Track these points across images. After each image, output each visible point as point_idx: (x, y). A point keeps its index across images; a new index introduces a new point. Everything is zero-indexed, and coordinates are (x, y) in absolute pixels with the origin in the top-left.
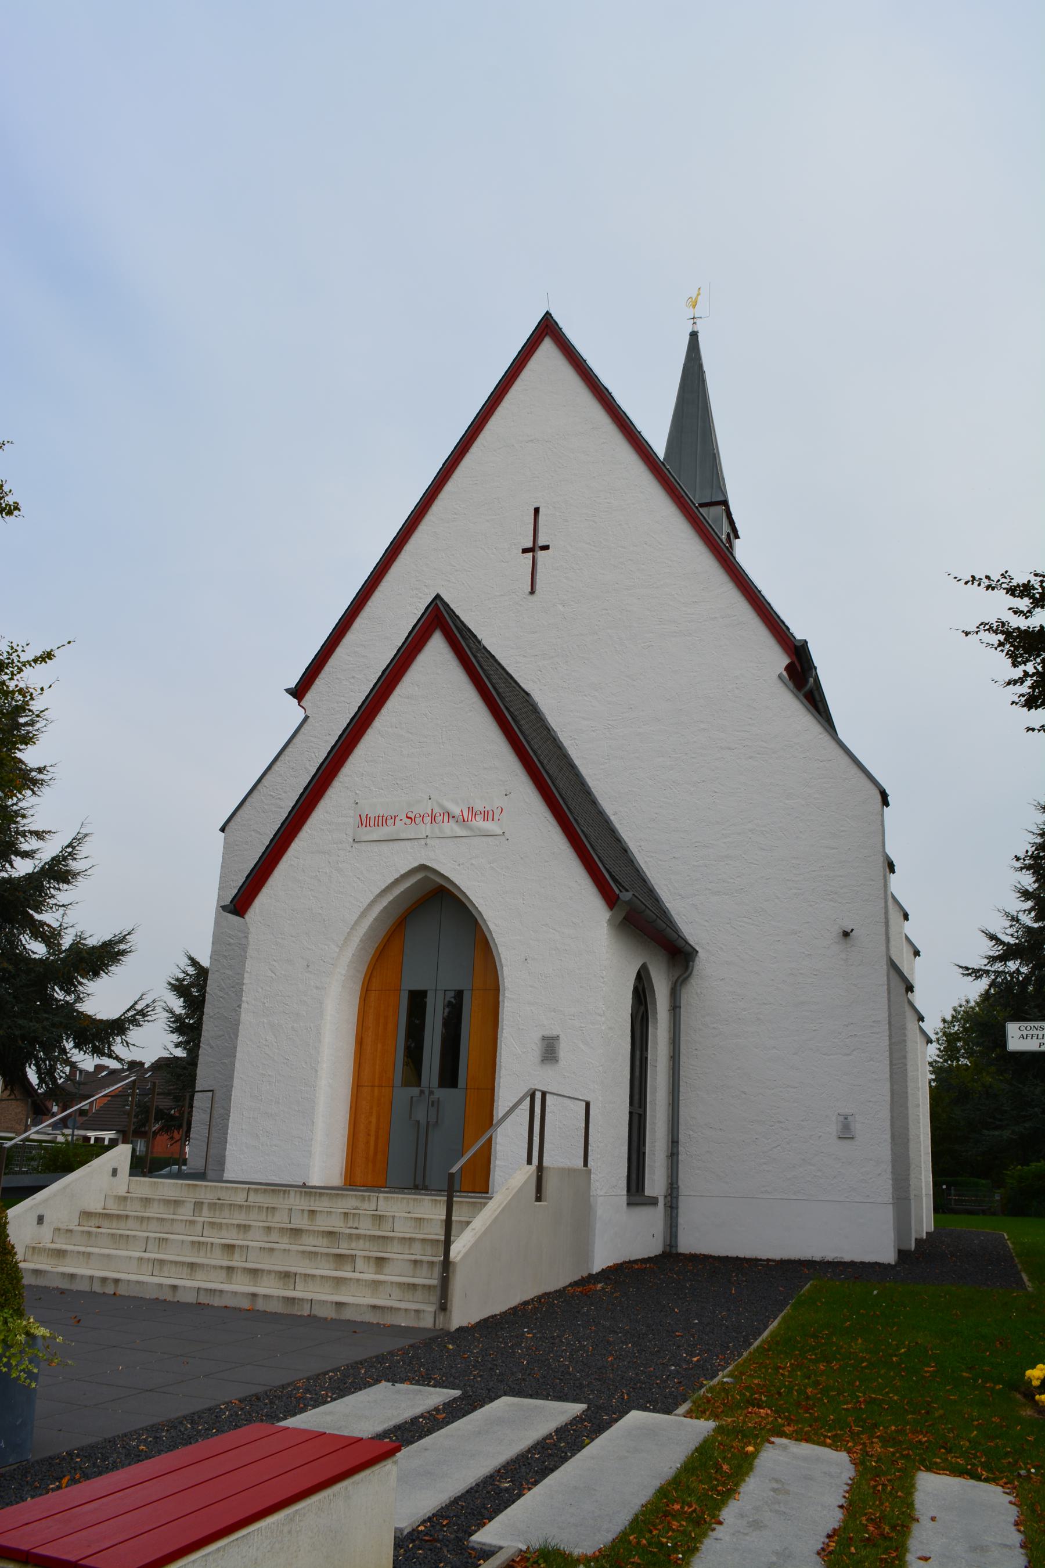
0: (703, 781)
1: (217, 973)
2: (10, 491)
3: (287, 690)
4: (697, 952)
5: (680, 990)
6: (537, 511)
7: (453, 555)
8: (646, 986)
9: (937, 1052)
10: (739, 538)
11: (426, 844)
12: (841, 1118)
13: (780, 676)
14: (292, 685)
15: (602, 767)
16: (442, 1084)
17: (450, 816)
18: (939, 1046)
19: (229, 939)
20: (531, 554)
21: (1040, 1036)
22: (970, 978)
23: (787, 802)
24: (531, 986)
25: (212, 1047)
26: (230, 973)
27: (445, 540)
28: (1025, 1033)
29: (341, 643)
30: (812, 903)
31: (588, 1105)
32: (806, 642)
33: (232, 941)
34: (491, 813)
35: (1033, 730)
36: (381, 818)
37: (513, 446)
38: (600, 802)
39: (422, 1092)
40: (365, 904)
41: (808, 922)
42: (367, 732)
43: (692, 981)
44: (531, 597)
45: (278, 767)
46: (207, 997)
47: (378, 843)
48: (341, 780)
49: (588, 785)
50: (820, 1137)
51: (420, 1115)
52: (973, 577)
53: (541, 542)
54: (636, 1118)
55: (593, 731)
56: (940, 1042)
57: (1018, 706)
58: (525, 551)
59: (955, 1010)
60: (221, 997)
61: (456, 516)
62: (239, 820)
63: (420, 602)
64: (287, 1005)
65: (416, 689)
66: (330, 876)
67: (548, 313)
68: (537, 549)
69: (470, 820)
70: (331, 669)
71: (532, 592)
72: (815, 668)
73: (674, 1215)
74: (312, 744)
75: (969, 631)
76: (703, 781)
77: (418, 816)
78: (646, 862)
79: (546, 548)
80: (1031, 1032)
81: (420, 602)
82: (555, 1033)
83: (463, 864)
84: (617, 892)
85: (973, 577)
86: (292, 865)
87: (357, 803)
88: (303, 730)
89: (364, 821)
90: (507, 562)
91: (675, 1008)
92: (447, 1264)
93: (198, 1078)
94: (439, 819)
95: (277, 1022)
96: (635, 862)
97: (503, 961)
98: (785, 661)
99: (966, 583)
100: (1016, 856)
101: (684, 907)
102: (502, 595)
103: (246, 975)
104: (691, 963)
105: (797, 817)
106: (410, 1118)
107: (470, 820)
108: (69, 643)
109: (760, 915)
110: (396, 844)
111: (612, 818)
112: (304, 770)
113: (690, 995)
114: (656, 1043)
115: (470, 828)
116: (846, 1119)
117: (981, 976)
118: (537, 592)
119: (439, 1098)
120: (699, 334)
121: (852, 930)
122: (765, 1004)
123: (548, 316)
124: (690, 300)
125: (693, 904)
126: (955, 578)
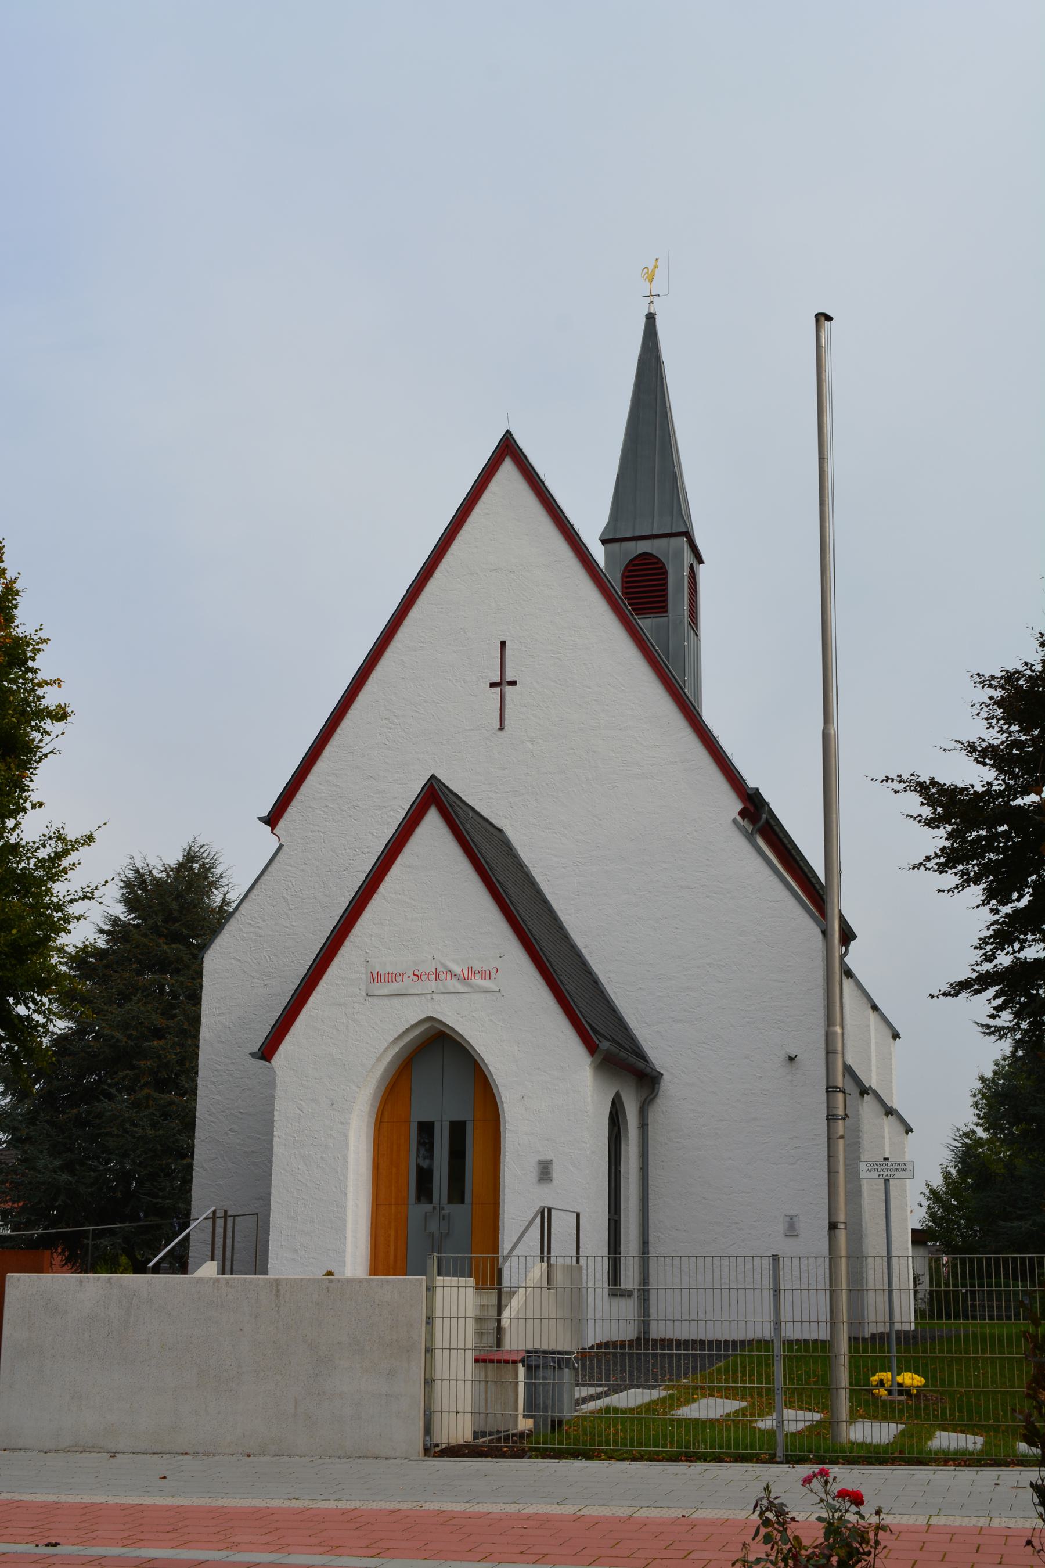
0: (666, 918)
1: (206, 1098)
2: (72, 712)
3: (261, 819)
4: (662, 1075)
5: (648, 1110)
6: (503, 644)
7: (421, 685)
8: (618, 1109)
9: (976, 1120)
10: (703, 563)
11: (432, 999)
12: (788, 1219)
13: (734, 821)
14: (265, 813)
15: (572, 902)
16: (450, 1201)
17: (452, 975)
18: (978, 1112)
19: (217, 1066)
20: (498, 689)
21: (879, 1170)
22: (993, 1038)
23: (741, 938)
24: (528, 1120)
25: (205, 1170)
26: (220, 1098)
27: (412, 669)
28: (870, 1168)
29: (312, 771)
30: (763, 1031)
31: (578, 1215)
32: (757, 790)
33: (219, 1067)
34: (488, 972)
35: (943, 891)
36: (390, 976)
37: (477, 574)
38: (572, 935)
39: (434, 1208)
40: (381, 1051)
41: (759, 1048)
42: (373, 897)
43: (658, 1101)
44: (500, 733)
45: (255, 896)
46: (197, 1122)
47: (389, 997)
48: (351, 940)
49: (560, 919)
50: (769, 1235)
51: (433, 1227)
52: (887, 777)
53: (509, 677)
54: (613, 1222)
55: (563, 867)
56: (980, 1106)
57: (930, 871)
58: (493, 685)
59: (997, 1064)
60: (212, 1122)
61: (422, 645)
62: (218, 948)
63: (390, 732)
64: (315, 1138)
65: (416, 859)
66: (347, 1026)
67: (508, 432)
68: (504, 682)
69: (470, 978)
70: (303, 797)
71: (501, 728)
72: (768, 804)
73: (646, 1306)
74: (290, 874)
75: (897, 789)
76: (666, 918)
77: (424, 973)
78: (614, 992)
79: (513, 683)
80: (874, 1167)
81: (390, 732)
82: (548, 1158)
83: (465, 1016)
84: (597, 1042)
85: (887, 777)
86: (311, 1016)
87: (368, 962)
88: (277, 858)
89: (375, 977)
90: (476, 696)
91: (644, 1126)
92: (499, 1329)
93: (193, 1199)
94: (443, 977)
95: (307, 1153)
96: (605, 993)
97: (503, 1099)
98: (739, 806)
99: (882, 782)
100: (930, 995)
101: (651, 1034)
102: (472, 729)
103: (276, 1113)
104: (657, 1085)
105: (749, 953)
106: (425, 1230)
107: (470, 978)
108: (105, 824)
109: (718, 1041)
110: (406, 999)
111: (583, 951)
112: (282, 899)
113: (658, 1113)
114: (628, 1158)
115: (470, 985)
116: (791, 1219)
117: (1005, 1035)
118: (506, 728)
119: (449, 1213)
120: (657, 317)
121: (796, 1056)
122: (722, 1120)
123: (508, 435)
124: (646, 270)
125: (658, 1031)
126: (872, 779)
